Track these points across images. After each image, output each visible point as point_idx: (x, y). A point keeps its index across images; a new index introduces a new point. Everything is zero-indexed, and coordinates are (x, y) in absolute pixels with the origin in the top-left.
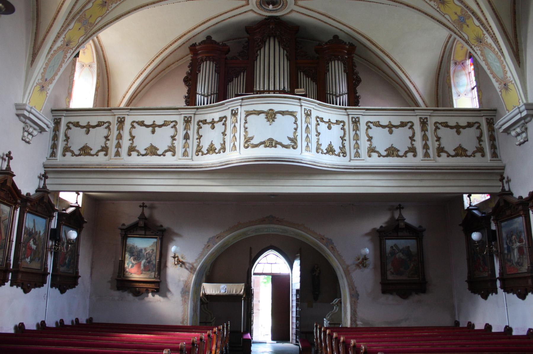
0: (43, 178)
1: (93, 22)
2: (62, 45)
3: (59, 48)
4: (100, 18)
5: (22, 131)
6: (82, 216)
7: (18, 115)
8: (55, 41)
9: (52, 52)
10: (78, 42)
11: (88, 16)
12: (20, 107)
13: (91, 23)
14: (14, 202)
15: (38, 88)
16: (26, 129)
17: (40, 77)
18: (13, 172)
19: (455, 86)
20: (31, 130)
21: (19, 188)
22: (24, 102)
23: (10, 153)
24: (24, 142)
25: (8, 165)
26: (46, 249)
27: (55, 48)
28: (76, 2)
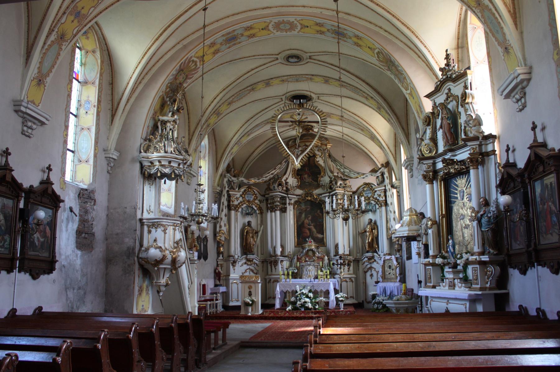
0: (47, 170)
5: (106, 166)
7: (16, 111)
8: (47, 37)
9: (46, 47)
10: (73, 34)
12: (17, 103)
13: (84, 15)
14: (55, 205)
16: (25, 124)
17: (36, 71)
18: (12, 168)
19: (365, 329)
20: (30, 124)
21: (20, 181)
22: (22, 99)
23: (50, 166)
24: (24, 136)
25: (48, 176)
26: (15, 232)
27: (49, 43)
28: (72, 2)
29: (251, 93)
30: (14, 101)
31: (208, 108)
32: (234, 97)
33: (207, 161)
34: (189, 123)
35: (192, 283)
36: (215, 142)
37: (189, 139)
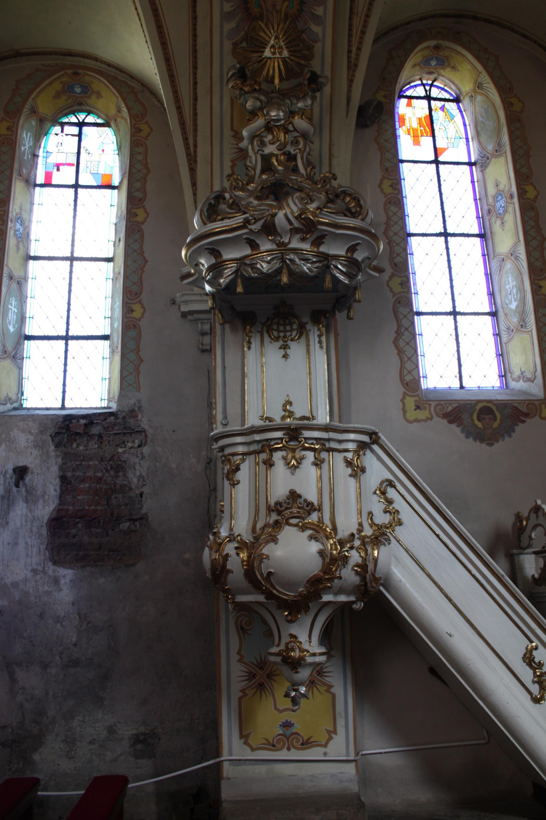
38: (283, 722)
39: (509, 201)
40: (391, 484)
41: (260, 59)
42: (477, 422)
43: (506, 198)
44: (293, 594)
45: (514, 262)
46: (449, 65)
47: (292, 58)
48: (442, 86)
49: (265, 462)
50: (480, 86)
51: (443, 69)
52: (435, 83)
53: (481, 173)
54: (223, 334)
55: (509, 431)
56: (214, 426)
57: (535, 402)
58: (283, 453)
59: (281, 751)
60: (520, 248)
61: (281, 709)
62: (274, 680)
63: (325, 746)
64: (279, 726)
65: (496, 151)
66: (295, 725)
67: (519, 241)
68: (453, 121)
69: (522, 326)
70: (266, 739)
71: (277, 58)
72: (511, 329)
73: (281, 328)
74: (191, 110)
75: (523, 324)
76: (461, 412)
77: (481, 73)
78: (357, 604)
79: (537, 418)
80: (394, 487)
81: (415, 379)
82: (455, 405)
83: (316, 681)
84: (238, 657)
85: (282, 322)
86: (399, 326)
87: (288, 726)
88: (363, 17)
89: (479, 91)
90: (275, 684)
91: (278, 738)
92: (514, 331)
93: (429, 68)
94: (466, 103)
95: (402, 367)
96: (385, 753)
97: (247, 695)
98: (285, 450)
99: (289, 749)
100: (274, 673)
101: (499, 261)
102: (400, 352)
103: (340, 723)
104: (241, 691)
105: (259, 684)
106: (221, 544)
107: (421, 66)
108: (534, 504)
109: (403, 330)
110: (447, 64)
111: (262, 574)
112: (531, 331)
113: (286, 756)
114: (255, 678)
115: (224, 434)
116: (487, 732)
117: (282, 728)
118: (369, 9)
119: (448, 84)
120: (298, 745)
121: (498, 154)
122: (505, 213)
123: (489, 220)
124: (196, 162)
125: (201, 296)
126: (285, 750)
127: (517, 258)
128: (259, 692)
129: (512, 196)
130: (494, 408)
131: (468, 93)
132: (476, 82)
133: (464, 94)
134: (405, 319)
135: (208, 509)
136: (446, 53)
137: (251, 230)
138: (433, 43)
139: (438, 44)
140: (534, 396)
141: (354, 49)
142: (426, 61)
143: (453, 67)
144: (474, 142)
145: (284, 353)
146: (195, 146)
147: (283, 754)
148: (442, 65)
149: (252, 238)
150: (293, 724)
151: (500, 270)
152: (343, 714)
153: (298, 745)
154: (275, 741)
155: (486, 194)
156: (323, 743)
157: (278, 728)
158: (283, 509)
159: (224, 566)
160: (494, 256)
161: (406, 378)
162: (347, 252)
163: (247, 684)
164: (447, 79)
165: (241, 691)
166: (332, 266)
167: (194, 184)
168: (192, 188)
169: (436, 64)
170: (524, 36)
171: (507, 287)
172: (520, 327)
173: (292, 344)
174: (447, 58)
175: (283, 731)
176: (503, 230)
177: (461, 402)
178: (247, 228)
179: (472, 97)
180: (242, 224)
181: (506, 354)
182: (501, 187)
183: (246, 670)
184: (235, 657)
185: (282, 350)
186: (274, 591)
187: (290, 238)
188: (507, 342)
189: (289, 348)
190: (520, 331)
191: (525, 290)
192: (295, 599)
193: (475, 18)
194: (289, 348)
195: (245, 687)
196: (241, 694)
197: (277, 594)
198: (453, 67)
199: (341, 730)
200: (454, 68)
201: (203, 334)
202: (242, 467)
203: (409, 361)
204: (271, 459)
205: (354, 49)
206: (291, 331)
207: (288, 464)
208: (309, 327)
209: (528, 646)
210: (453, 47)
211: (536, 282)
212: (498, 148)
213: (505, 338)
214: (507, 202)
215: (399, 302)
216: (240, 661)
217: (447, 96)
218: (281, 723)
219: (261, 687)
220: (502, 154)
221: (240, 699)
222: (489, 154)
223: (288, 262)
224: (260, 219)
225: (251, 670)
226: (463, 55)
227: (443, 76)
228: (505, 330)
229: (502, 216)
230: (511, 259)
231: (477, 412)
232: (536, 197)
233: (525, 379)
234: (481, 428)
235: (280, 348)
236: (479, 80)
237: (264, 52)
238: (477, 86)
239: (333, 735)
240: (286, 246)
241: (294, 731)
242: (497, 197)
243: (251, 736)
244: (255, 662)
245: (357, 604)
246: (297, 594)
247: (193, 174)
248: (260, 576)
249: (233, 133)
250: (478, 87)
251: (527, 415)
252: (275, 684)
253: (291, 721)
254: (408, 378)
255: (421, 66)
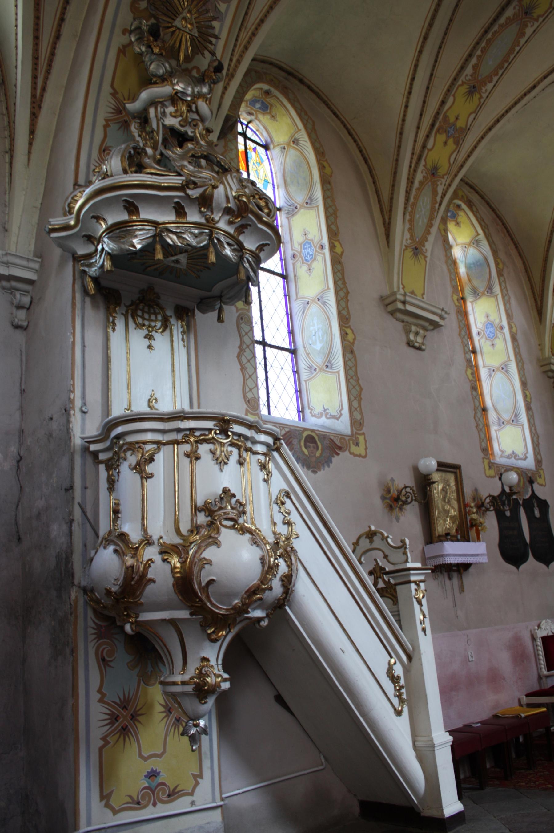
1: (464, 126)
2: (424, 177)
3: (421, 183)
4: (473, 116)
6: (420, 650)
7: (392, 313)
10: (454, 96)
11: (452, 119)
12: (388, 301)
15: (409, 253)
29: (529, 31)
30: (382, 299)
31: (405, 115)
32: (474, 61)
33: (500, 296)
34: (374, 182)
35: (410, 658)
36: (516, 247)
37: (384, 223)
38: (148, 772)
39: (318, 250)
40: (288, 495)
41: (170, 25)
42: (304, 449)
43: (315, 247)
44: (225, 607)
45: (321, 306)
46: (270, 113)
47: (199, 39)
48: (255, 130)
49: (187, 455)
50: (296, 142)
51: (264, 114)
52: (250, 125)
53: (286, 220)
54: (83, 308)
55: (328, 462)
56: (72, 412)
57: (345, 437)
58: (211, 446)
59: (147, 809)
60: (329, 295)
61: (146, 755)
62: (139, 722)
63: (192, 794)
64: (144, 778)
65: (307, 203)
66: (161, 774)
67: (328, 288)
68: (262, 165)
69: (327, 366)
70: (131, 797)
71: (186, 32)
72: (314, 368)
73: (146, 316)
74: (50, 47)
75: (328, 366)
76: (291, 437)
77: (300, 130)
78: (264, 621)
79: (347, 453)
80: (290, 498)
81: (255, 398)
82: (287, 430)
83: (182, 718)
84: (99, 696)
85: (146, 309)
86: (242, 342)
87: (153, 775)
88: (250, 33)
89: (294, 146)
90: (139, 725)
91: (143, 792)
92: (317, 370)
93: (252, 109)
94: (275, 152)
95: (244, 384)
96: (243, 792)
97: (109, 743)
98: (213, 443)
99: (154, 805)
100: (139, 713)
101: (303, 303)
102: (243, 369)
103: (206, 764)
104: (102, 739)
105: (122, 727)
106: (137, 548)
107: (247, 103)
108: (368, 529)
109: (245, 347)
110: (269, 111)
111: (200, 583)
112: (338, 372)
113: (152, 814)
114: (117, 721)
115: (138, 417)
116: (324, 757)
117: (147, 779)
118: (256, 29)
119: (261, 130)
120: (164, 798)
121: (308, 206)
122: (313, 260)
123: (293, 264)
124: (40, 107)
125: (28, 261)
126: (151, 806)
127: (324, 303)
128: (122, 737)
129: (322, 247)
130: (316, 438)
131: (281, 144)
132: (292, 136)
133: (276, 144)
134: (246, 336)
135: (16, 517)
136: (273, 101)
137: (188, 195)
138: (266, 87)
139: (269, 90)
140: (337, 431)
141: (235, 59)
142: (253, 101)
143: (273, 116)
144: (280, 190)
145: (149, 344)
146: (44, 89)
147: (149, 812)
148: (264, 110)
149: (183, 204)
150: (159, 772)
151: (303, 312)
152: (208, 753)
153: (164, 798)
154: (140, 797)
155: (291, 239)
156: (190, 791)
157: (143, 780)
158: (217, 508)
159: (144, 574)
160: (297, 298)
161: (248, 395)
162: (257, 249)
163: (110, 728)
164: (262, 125)
165: (102, 739)
166: (245, 259)
167: (32, 132)
168: (30, 135)
169: (260, 108)
170: (335, 114)
171: (312, 328)
172: (325, 367)
173: (157, 336)
174: (271, 105)
175: (148, 783)
176: (310, 275)
177: (292, 428)
178: (185, 192)
179: (284, 148)
180: (180, 185)
181: (305, 391)
182: (310, 236)
183: (108, 712)
184: (95, 696)
185: (147, 340)
186: (208, 604)
187: (220, 217)
188: (308, 380)
189: (154, 340)
190: (324, 370)
191: (333, 333)
192: (228, 613)
193: (301, 81)
194: (154, 340)
195: (106, 734)
196: (102, 743)
197: (210, 607)
198: (273, 116)
199: (207, 773)
200: (273, 117)
201: (19, 307)
202: (156, 457)
203: (250, 379)
204: (196, 451)
205: (235, 59)
206: (156, 320)
207: (217, 459)
208: (173, 321)
209: (390, 661)
210: (281, 99)
211: (344, 328)
212: (309, 201)
213: (304, 375)
214: (316, 251)
215: (242, 319)
216: (101, 701)
217: (259, 141)
218: (146, 774)
219: (125, 731)
220: (314, 207)
221: (101, 749)
222: (298, 204)
223: (216, 241)
224: (201, 187)
225: (114, 711)
226: (287, 110)
227: (260, 121)
228: (307, 368)
229: (309, 263)
230: (317, 304)
231: (304, 439)
232: (342, 253)
233: (328, 416)
234: (307, 455)
235: (145, 337)
236: (296, 136)
237: (174, 20)
238: (292, 140)
239: (199, 780)
240: (214, 224)
241: (159, 781)
242: (305, 245)
243: (114, 792)
244: (118, 701)
245: (264, 621)
246: (231, 607)
247: (34, 120)
248: (198, 585)
249: (112, 91)
250: (294, 142)
251: (340, 448)
252: (139, 725)
253: (148, 772)
254: (250, 395)
255: (247, 103)
